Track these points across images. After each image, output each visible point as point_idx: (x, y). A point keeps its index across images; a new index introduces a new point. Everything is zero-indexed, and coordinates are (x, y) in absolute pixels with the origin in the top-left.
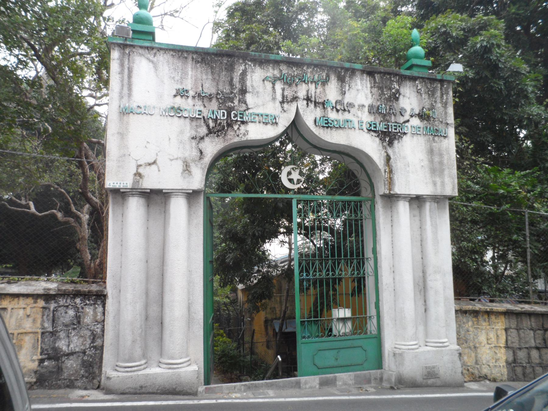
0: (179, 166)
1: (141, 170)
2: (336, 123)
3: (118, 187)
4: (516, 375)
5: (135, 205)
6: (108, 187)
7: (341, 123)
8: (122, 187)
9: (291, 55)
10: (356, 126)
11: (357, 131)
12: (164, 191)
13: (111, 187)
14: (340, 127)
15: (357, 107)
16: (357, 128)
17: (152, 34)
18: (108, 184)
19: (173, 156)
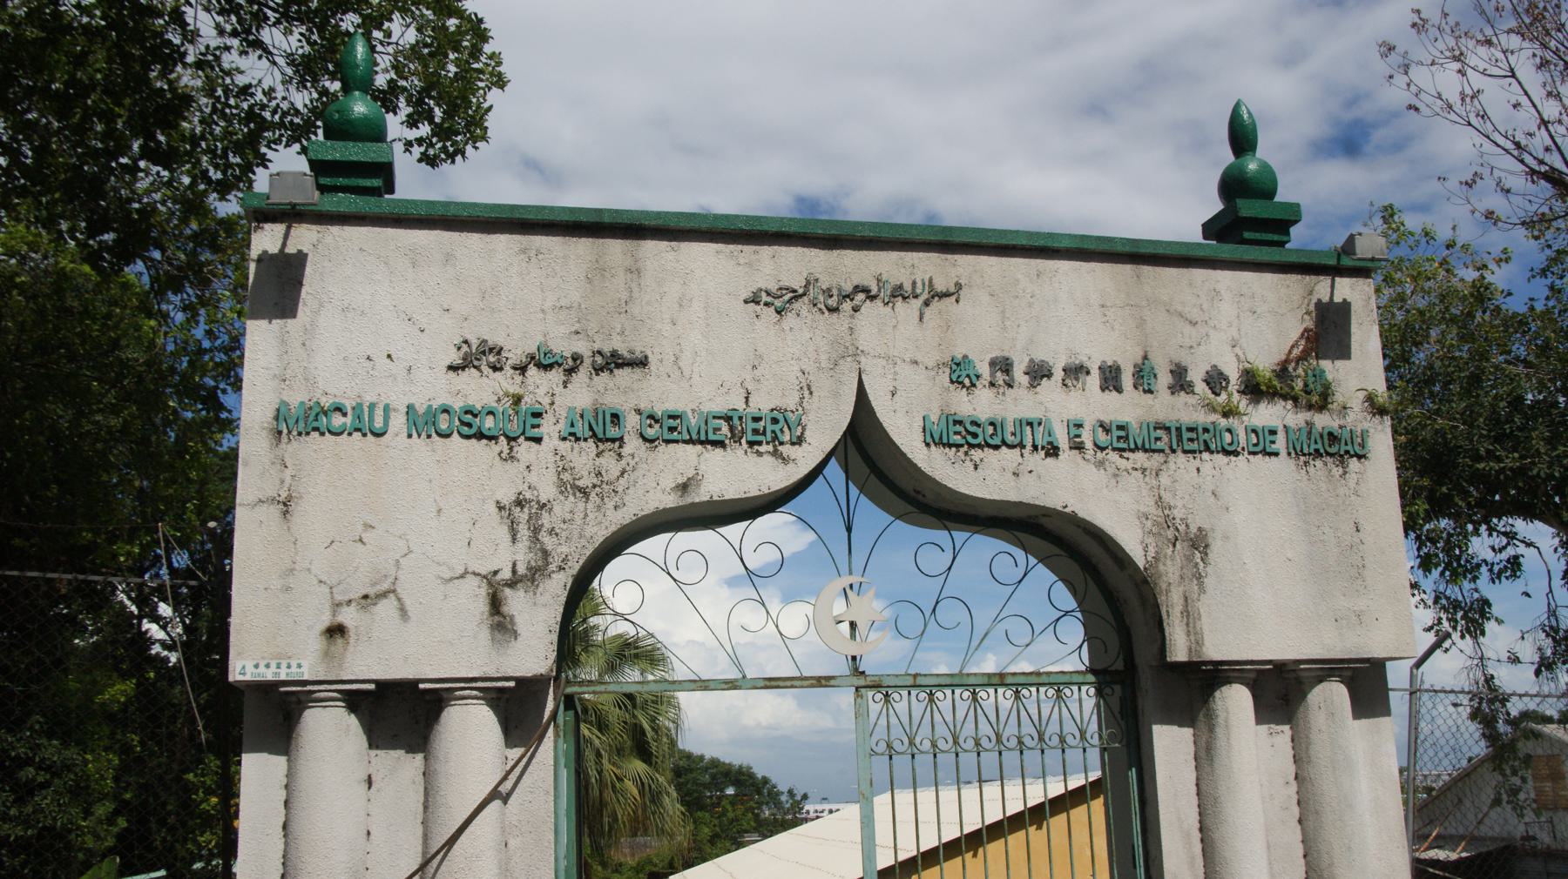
0: (473, 597)
1: (348, 617)
2: (990, 430)
3: (270, 677)
4: (637, 656)
5: (330, 732)
6: (240, 678)
7: (1009, 428)
8: (283, 677)
9: (170, 807)
10: (1062, 440)
11: (1066, 454)
12: (421, 686)
13: (248, 678)
14: (1004, 443)
15: (1058, 374)
16: (1089, 445)
17: (384, 172)
18: (238, 670)
19: (451, 569)
